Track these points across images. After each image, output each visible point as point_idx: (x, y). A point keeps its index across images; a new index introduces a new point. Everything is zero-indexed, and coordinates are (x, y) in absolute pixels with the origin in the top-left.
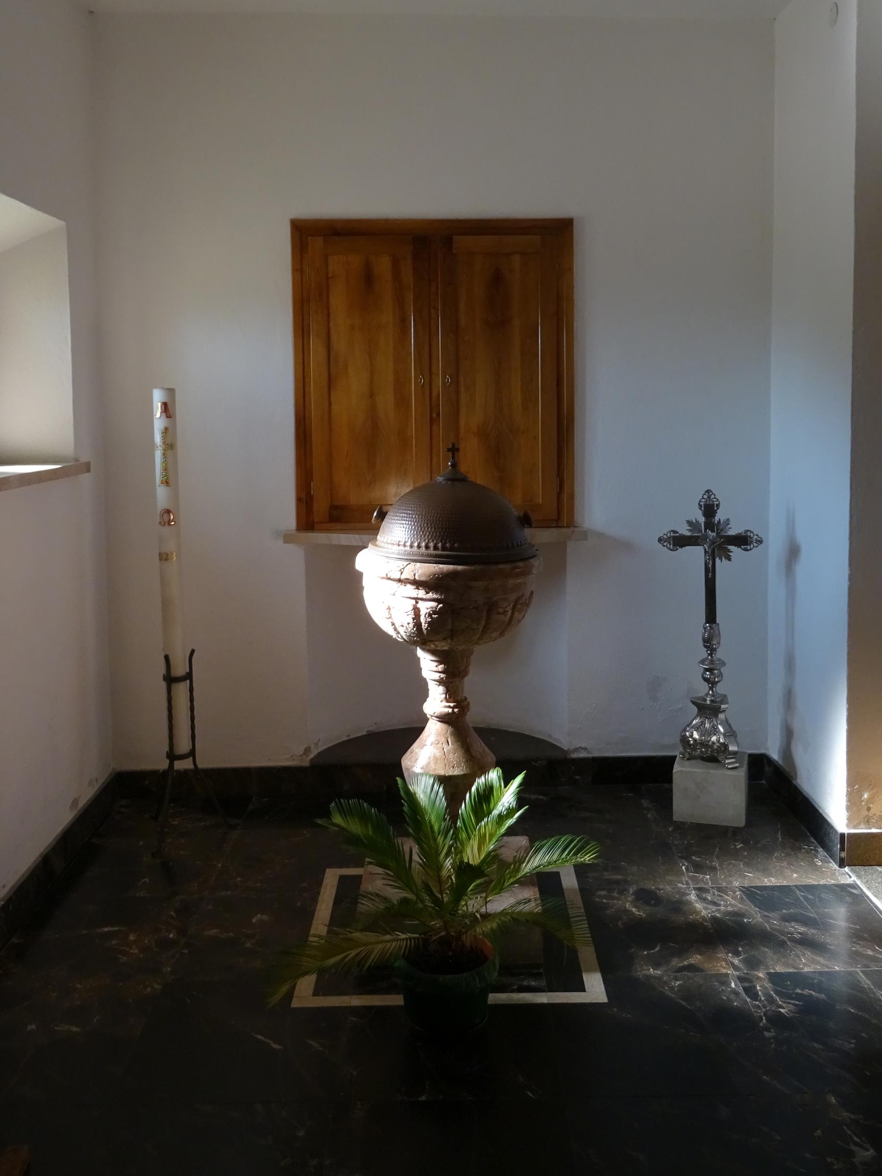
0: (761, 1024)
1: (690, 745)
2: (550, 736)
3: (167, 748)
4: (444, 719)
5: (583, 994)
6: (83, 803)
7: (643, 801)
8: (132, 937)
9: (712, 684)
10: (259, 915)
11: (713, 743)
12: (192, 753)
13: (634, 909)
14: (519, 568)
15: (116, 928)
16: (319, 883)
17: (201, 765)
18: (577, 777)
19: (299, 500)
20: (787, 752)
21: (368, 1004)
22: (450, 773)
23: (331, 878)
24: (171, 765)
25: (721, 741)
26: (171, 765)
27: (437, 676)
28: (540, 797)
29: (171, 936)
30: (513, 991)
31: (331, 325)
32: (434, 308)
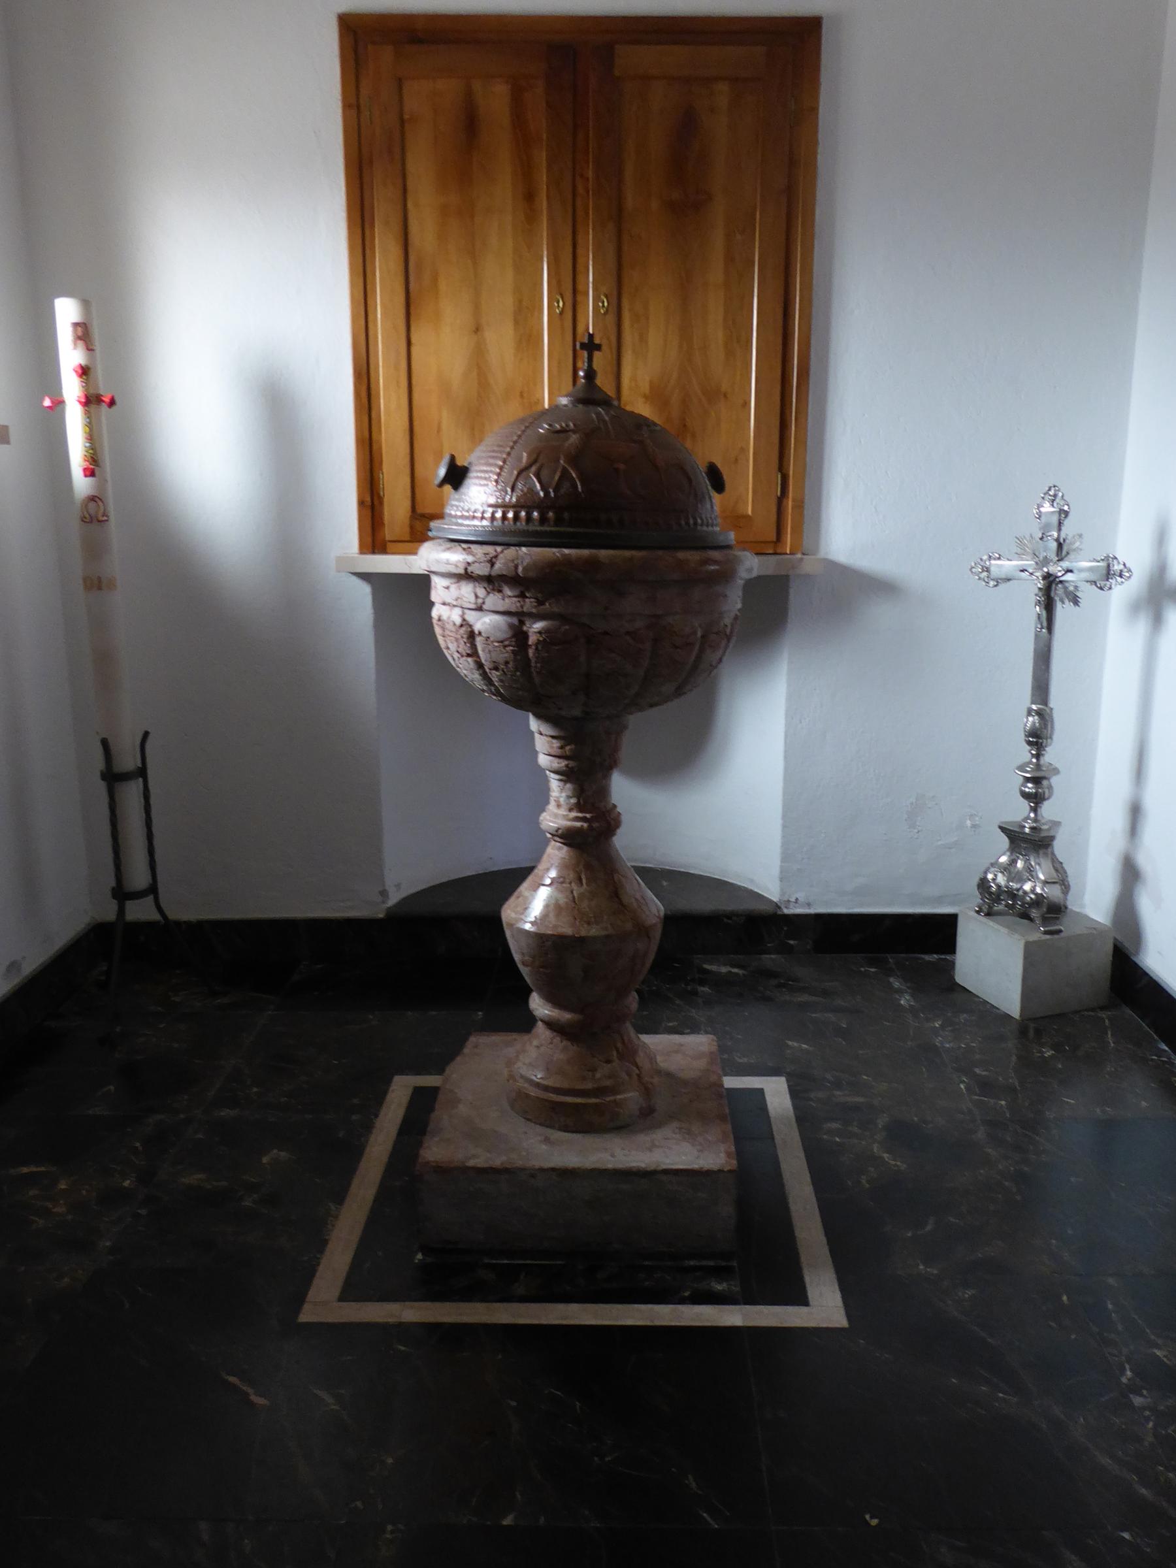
0: (1124, 1380)
1: (991, 893)
2: (752, 881)
3: (113, 883)
4: (568, 837)
5: (804, 1309)
6: (29, 967)
7: (892, 980)
8: (63, 1186)
9: (1036, 799)
10: (275, 1151)
11: (1025, 893)
12: (153, 890)
13: (886, 1156)
14: (715, 562)
15: (43, 1169)
16: (379, 1098)
17: (180, 912)
18: (792, 942)
19: (361, 503)
20: (1126, 910)
21: (431, 1319)
22: (583, 933)
23: (401, 1089)
24: (121, 911)
25: (1038, 890)
26: (121, 911)
27: (558, 764)
28: (735, 970)
29: (127, 1183)
30: (682, 1301)
31: (410, 205)
32: (582, 176)
